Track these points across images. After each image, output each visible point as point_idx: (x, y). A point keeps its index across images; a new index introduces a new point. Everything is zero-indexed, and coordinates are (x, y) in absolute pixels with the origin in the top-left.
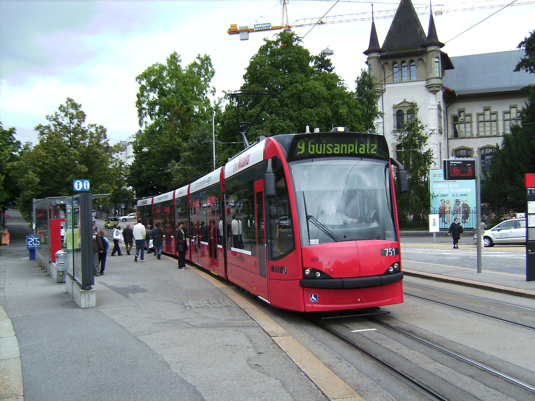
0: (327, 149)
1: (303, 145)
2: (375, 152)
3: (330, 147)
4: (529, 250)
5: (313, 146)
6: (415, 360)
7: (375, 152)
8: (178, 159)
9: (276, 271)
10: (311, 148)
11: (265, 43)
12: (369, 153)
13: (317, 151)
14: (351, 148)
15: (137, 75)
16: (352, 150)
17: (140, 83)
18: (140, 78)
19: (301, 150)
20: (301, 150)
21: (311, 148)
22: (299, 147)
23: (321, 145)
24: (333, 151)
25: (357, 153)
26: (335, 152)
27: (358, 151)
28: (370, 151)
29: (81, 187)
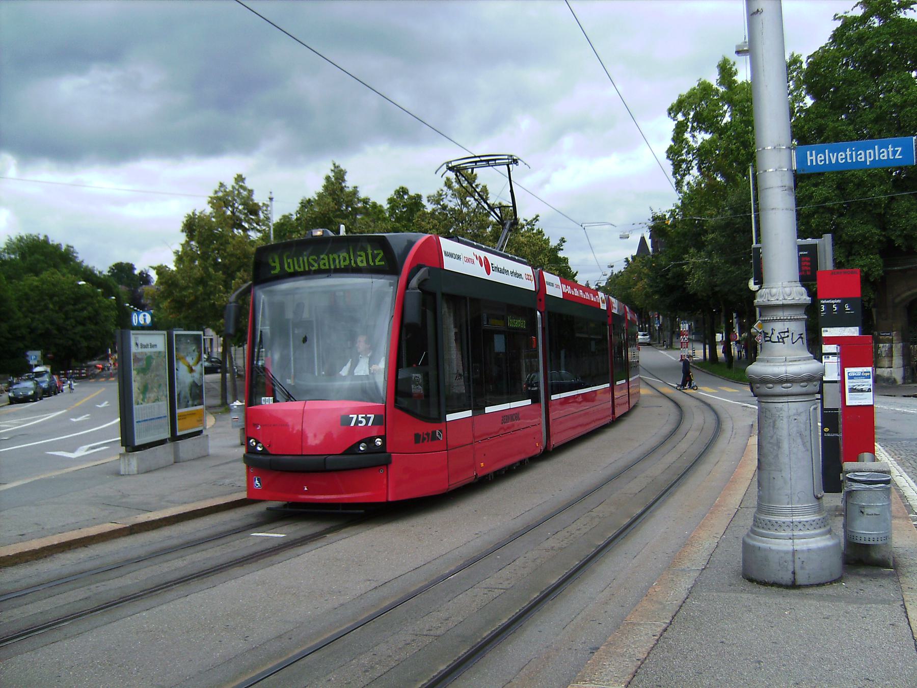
0: (310, 264)
1: (277, 260)
2: (383, 263)
3: (314, 260)
4: (826, 430)
5: (290, 260)
6: (199, 555)
7: (383, 263)
8: (700, 246)
9: (424, 439)
10: (289, 264)
11: (839, 24)
12: (372, 264)
13: (296, 268)
14: (345, 260)
15: (669, 106)
16: (347, 262)
17: (674, 119)
18: (673, 111)
19: (274, 268)
20: (274, 268)
21: (289, 264)
22: (273, 264)
23: (301, 259)
24: (319, 265)
25: (372, 264)
26: (322, 267)
27: (356, 262)
28: (374, 261)
29: (141, 316)
